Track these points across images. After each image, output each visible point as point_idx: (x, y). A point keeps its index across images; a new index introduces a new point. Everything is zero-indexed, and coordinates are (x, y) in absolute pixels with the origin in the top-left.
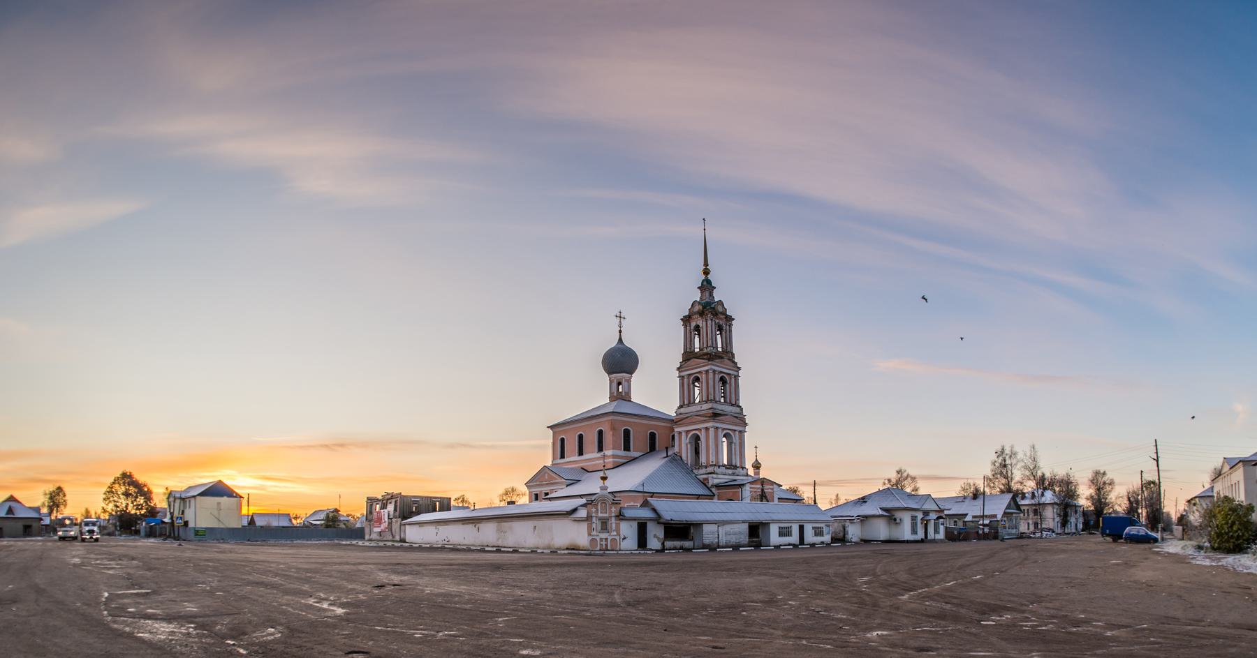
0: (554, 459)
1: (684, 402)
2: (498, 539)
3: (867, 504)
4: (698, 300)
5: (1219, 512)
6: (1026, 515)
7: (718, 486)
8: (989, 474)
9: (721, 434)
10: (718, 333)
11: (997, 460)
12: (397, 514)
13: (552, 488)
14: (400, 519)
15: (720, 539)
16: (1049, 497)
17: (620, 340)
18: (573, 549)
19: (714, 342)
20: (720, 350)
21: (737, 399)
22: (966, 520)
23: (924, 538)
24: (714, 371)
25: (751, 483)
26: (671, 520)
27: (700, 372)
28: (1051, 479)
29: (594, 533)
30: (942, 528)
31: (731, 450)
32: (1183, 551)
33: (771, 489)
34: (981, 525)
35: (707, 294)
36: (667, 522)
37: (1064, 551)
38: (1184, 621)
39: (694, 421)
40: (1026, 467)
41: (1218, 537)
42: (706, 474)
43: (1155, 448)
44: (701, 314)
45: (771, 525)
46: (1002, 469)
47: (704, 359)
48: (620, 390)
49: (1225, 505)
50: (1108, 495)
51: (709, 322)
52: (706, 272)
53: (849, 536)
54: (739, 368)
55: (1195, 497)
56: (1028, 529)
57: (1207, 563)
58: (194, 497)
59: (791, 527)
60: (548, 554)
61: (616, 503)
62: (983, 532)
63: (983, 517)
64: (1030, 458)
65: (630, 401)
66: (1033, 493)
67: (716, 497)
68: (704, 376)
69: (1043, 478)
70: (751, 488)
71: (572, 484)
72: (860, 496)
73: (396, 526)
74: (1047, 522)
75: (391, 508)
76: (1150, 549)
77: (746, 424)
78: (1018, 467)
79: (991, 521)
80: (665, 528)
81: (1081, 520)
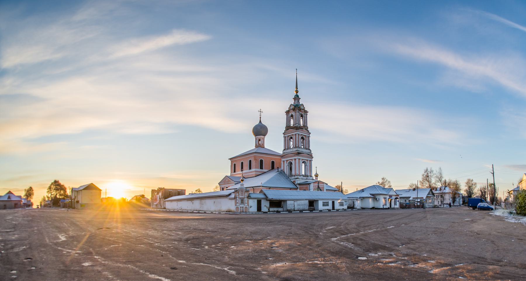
0: (231, 173)
1: (286, 148)
2: (200, 208)
3: (364, 192)
4: (293, 104)
5: (520, 197)
6: (437, 197)
7: (299, 184)
8: (421, 180)
9: (301, 162)
10: (301, 118)
11: (424, 174)
12: (163, 197)
13: (229, 185)
14: (164, 199)
15: (295, 207)
16: (447, 190)
17: (260, 121)
18: (229, 212)
19: (299, 122)
20: (302, 125)
21: (309, 146)
22: (410, 199)
23: (389, 207)
24: (299, 134)
25: (314, 183)
26: (272, 199)
27: (293, 135)
28: (449, 182)
29: (238, 204)
30: (398, 203)
31: (306, 168)
32: (503, 215)
33: (322, 185)
34: (416, 202)
35: (297, 101)
36: (270, 199)
37: (446, 214)
38: (489, 261)
39: (290, 156)
40: (437, 177)
41: (520, 208)
42: (294, 179)
43: (492, 168)
44: (294, 110)
45: (319, 201)
46: (427, 178)
47: (294, 129)
48: (260, 143)
49: (523, 193)
50: (474, 189)
51: (297, 113)
52: (297, 92)
53: (356, 206)
54: (310, 133)
55: (512, 191)
56: (438, 204)
57: (513, 221)
58: (81, 190)
59: (328, 202)
60: (217, 214)
61: (247, 191)
62: (417, 205)
63: (417, 198)
64: (439, 173)
65: (264, 148)
66: (440, 188)
67: (299, 189)
68: (294, 136)
69: (445, 182)
70: (313, 185)
71: (238, 183)
72: (362, 189)
73: (162, 202)
74: (446, 201)
75: (160, 194)
76: (488, 213)
77: (313, 157)
78: (434, 177)
79: (421, 200)
80: (270, 202)
81: (461, 200)
